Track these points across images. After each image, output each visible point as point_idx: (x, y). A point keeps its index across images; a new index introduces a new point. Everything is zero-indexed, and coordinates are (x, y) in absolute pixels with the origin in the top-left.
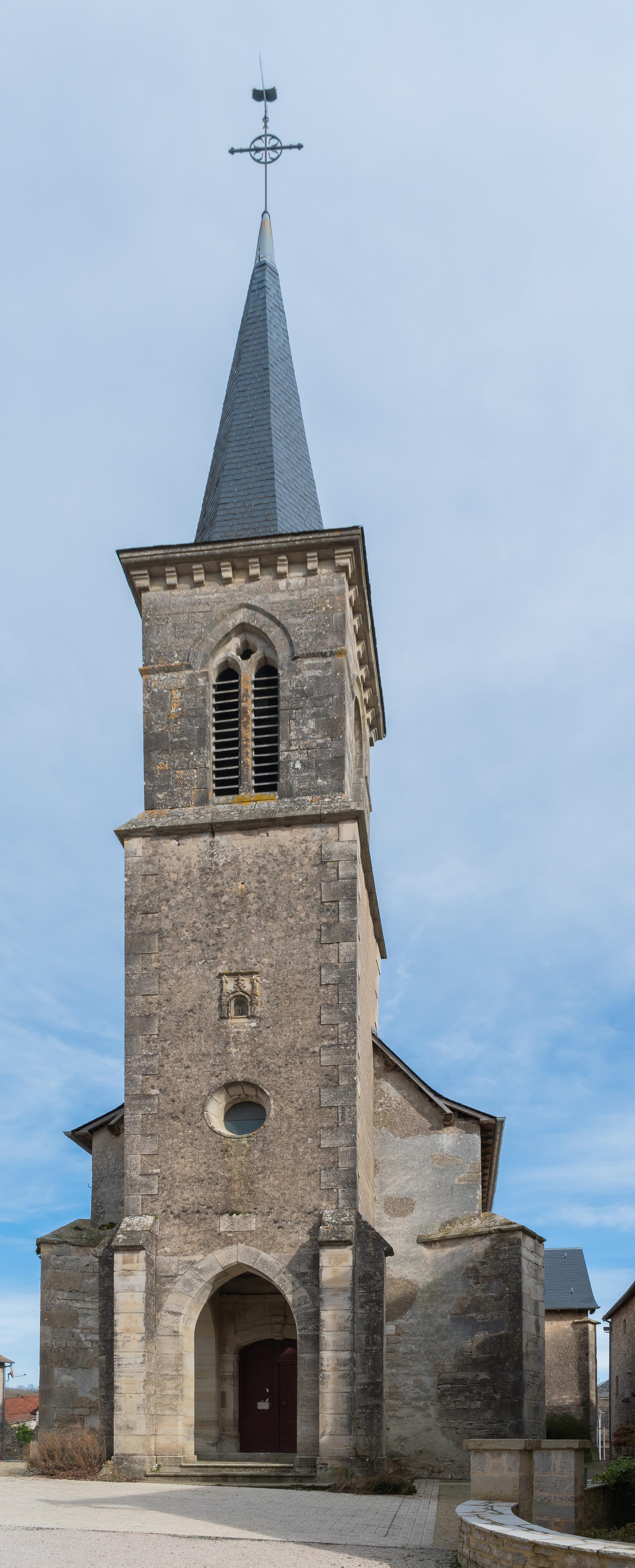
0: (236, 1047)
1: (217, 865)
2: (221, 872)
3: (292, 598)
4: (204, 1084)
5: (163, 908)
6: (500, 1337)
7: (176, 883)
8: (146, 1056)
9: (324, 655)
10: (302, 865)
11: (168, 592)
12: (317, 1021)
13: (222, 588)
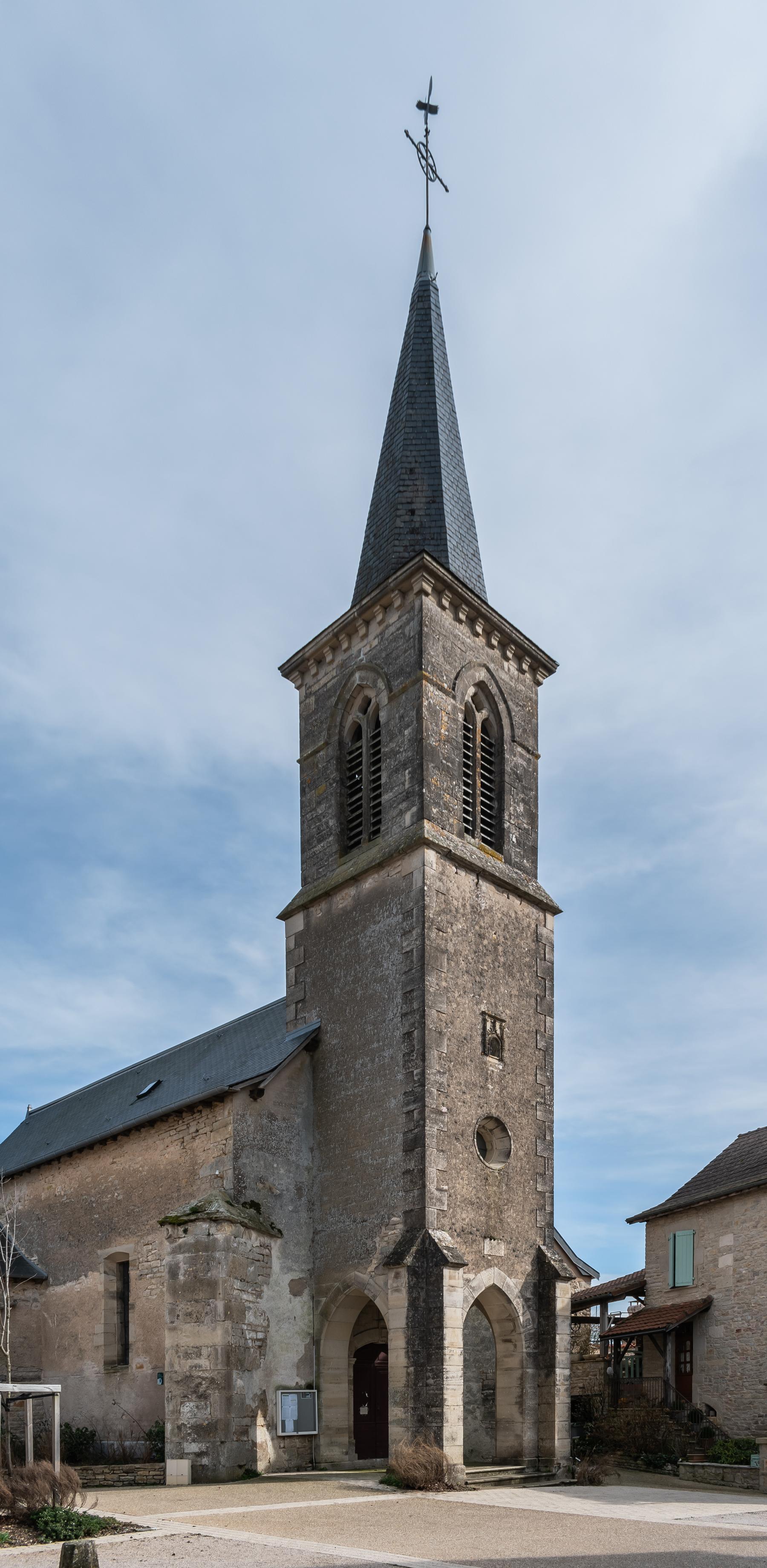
2: (482, 916)
7: (457, 911)
9: (528, 751)
11: (439, 609)
13: (472, 636)
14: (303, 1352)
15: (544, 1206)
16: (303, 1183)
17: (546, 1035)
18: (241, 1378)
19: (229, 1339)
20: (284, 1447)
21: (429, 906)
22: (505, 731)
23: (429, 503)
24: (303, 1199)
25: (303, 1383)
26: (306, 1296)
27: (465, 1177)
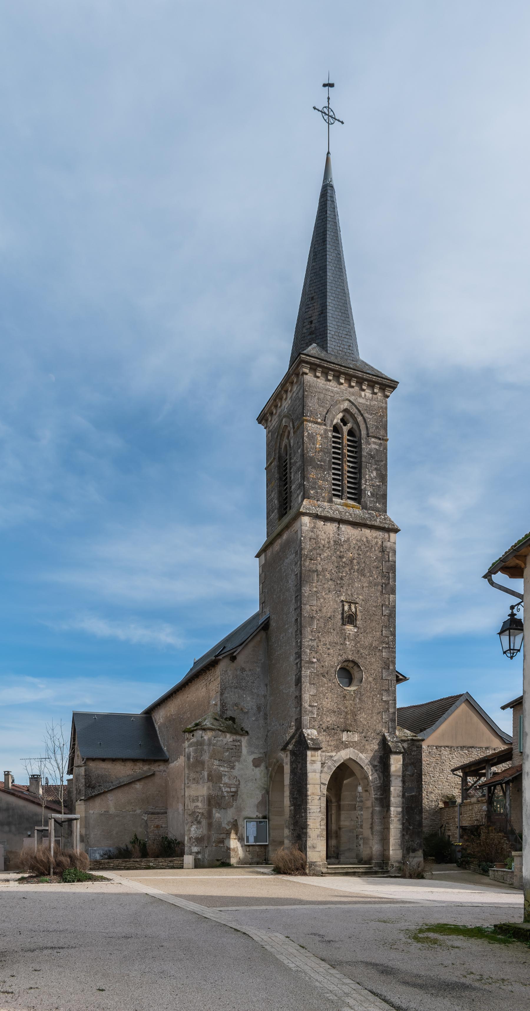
0: (349, 642)
1: (341, 541)
2: (342, 545)
3: (367, 403)
4: (336, 659)
5: (318, 558)
6: (412, 796)
7: (324, 546)
8: (311, 640)
9: (380, 439)
10: (375, 550)
11: (315, 379)
12: (381, 633)
13: (338, 386)
14: (261, 798)
15: (388, 709)
16: (261, 704)
17: (390, 606)
18: (219, 813)
19: (211, 792)
20: (249, 851)
21: (304, 548)
22: (362, 433)
23: (320, 314)
24: (261, 713)
25: (260, 815)
26: (263, 767)
27: (329, 697)
